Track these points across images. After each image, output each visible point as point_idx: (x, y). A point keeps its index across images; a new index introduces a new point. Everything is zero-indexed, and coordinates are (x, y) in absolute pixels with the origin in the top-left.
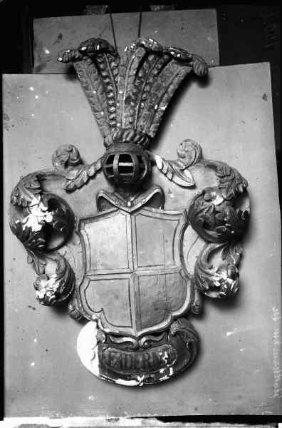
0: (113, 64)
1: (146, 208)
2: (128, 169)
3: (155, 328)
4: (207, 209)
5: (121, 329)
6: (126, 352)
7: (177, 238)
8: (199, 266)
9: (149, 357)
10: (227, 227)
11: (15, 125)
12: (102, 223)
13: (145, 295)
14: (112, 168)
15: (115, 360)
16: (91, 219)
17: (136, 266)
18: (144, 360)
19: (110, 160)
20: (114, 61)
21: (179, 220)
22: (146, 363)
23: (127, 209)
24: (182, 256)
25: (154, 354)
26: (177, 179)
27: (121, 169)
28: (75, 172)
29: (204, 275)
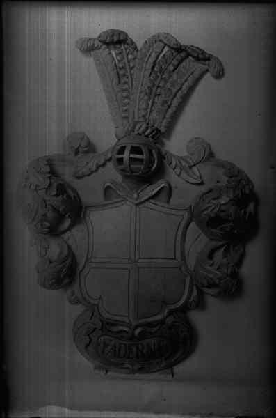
3: (150, 320)
4: (212, 208)
14: (122, 159)
19: (122, 151)
26: (184, 175)
27: (131, 159)
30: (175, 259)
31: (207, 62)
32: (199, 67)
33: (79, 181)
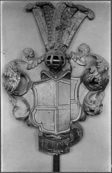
0: (51, 11)
1: (63, 79)
2: (58, 63)
3: (64, 132)
4: (91, 77)
5: (49, 131)
6: (51, 141)
7: (77, 86)
8: (85, 100)
9: (61, 143)
10: (99, 85)
11: (49, 114)
12: (42, 85)
13: (61, 117)
14: (50, 61)
15: (46, 144)
16: (38, 83)
17: (57, 105)
18: (59, 145)
19: (49, 58)
20: (51, 10)
21: (78, 80)
22: (60, 146)
23: (55, 80)
24: (78, 96)
25: (63, 143)
26: (78, 62)
27: (54, 62)
28: (31, 62)
29: (88, 105)
30: (75, 100)
31: (86, 13)
32: (82, 15)
33: (28, 70)
